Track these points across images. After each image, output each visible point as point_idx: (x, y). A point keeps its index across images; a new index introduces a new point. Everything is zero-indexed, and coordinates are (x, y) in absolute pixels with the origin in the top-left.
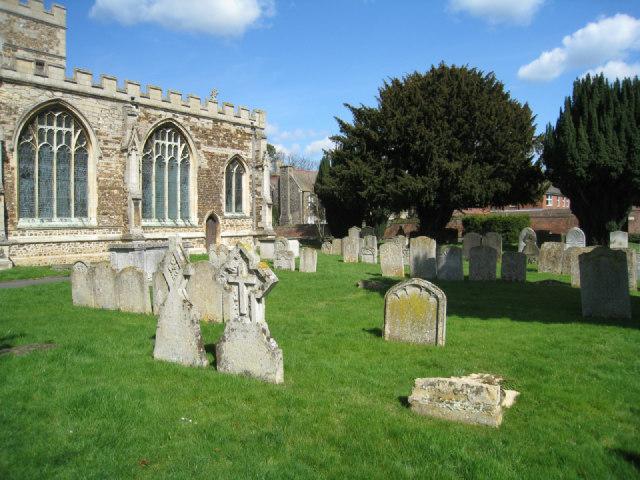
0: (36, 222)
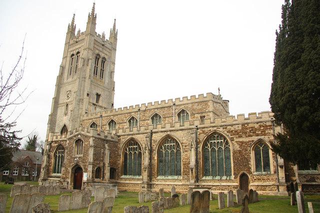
0: (163, 177)
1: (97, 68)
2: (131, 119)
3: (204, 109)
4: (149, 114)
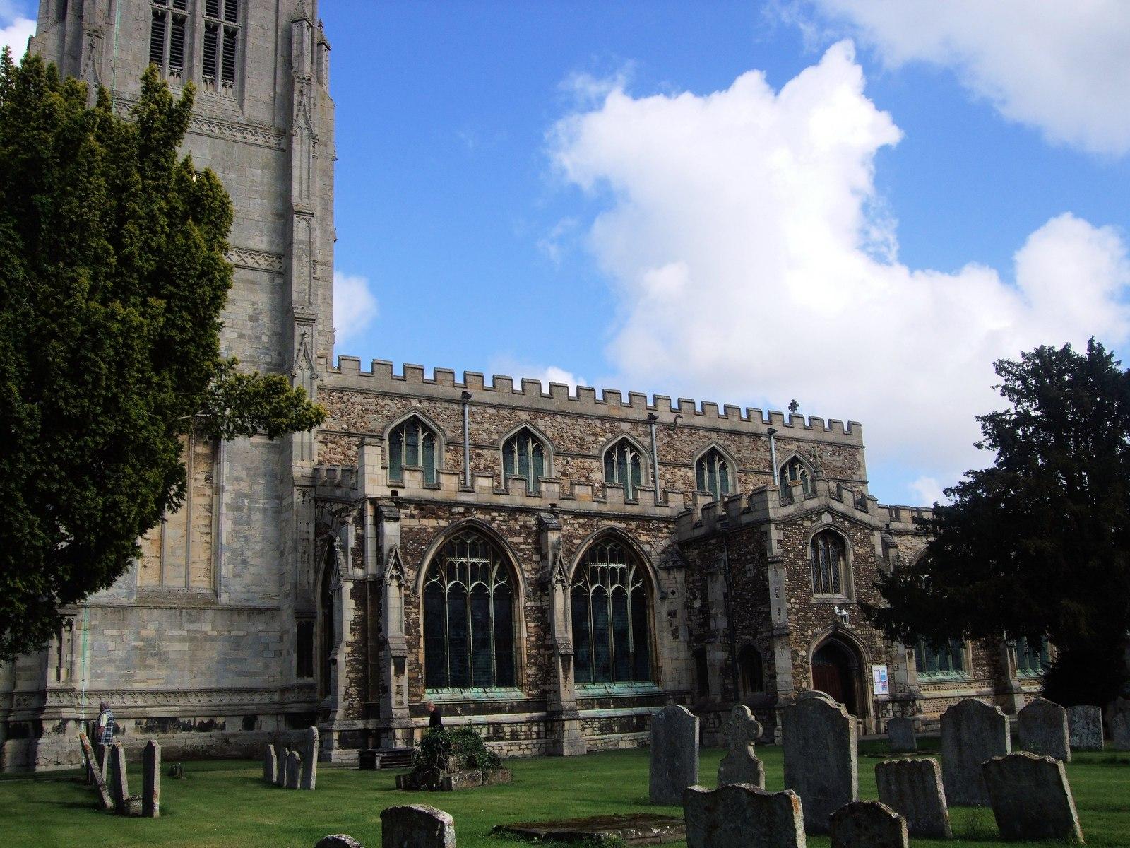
3: (849, 472)
4: (695, 447)
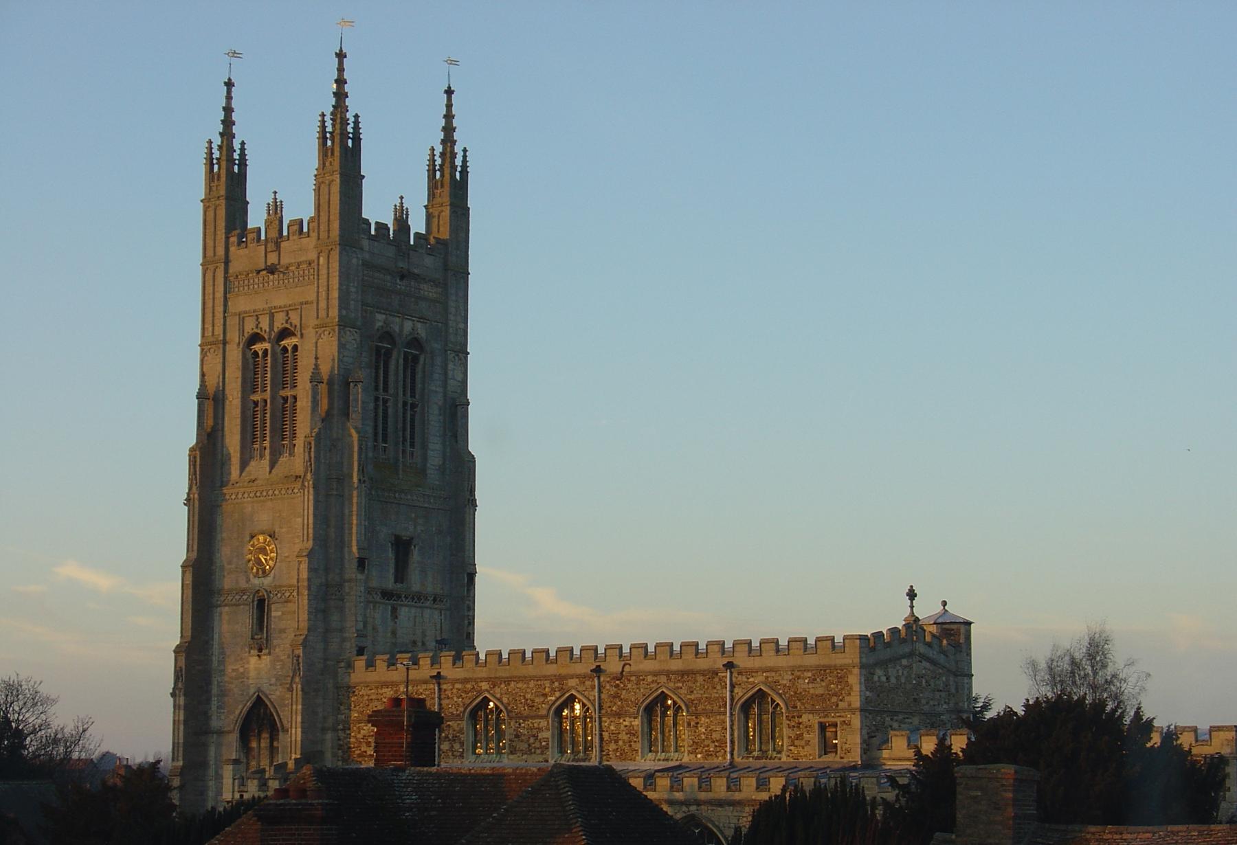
1: (385, 401)
2: (654, 701)
3: (834, 699)
4: (638, 695)
